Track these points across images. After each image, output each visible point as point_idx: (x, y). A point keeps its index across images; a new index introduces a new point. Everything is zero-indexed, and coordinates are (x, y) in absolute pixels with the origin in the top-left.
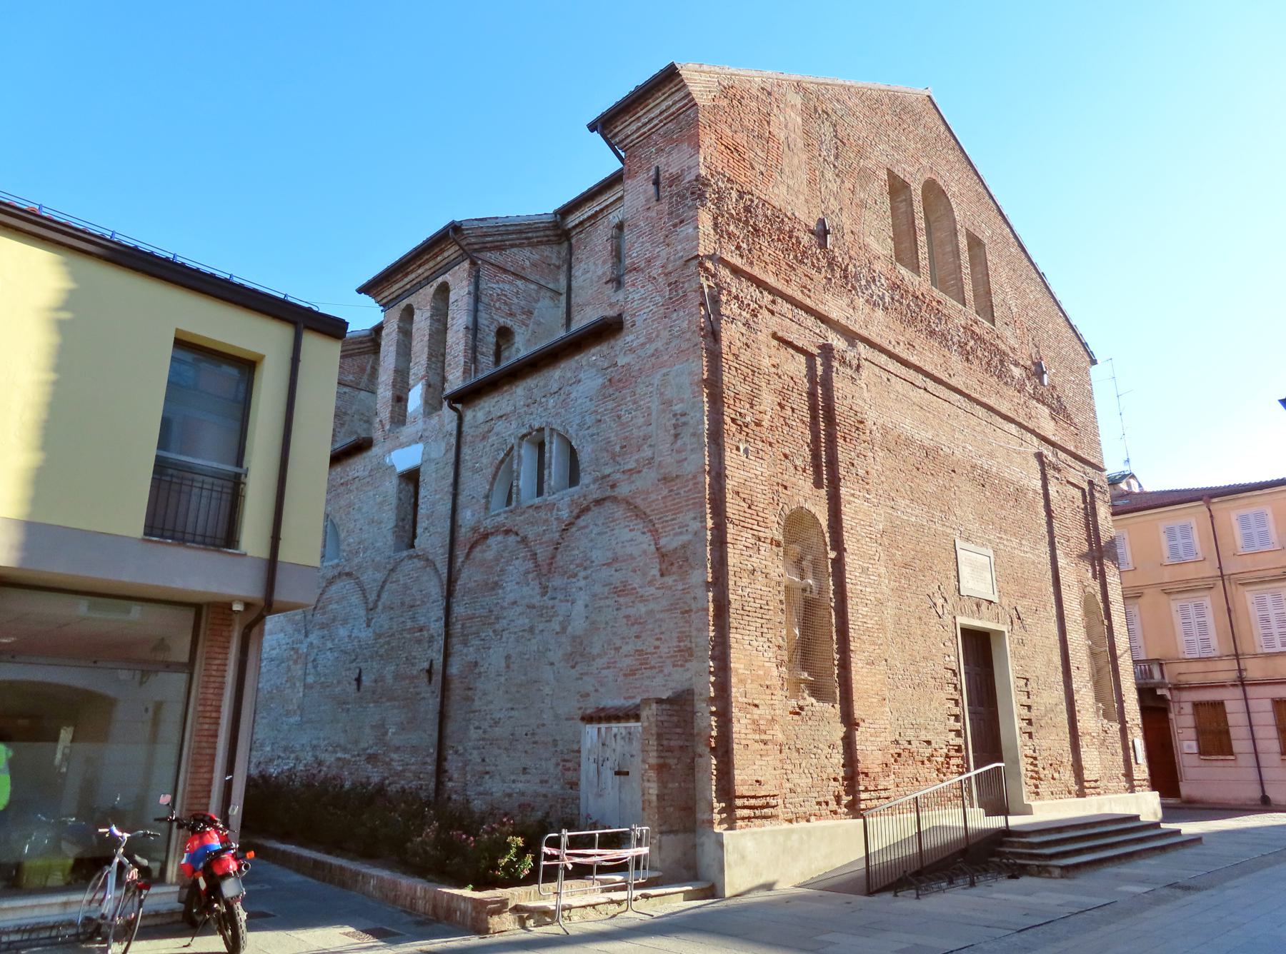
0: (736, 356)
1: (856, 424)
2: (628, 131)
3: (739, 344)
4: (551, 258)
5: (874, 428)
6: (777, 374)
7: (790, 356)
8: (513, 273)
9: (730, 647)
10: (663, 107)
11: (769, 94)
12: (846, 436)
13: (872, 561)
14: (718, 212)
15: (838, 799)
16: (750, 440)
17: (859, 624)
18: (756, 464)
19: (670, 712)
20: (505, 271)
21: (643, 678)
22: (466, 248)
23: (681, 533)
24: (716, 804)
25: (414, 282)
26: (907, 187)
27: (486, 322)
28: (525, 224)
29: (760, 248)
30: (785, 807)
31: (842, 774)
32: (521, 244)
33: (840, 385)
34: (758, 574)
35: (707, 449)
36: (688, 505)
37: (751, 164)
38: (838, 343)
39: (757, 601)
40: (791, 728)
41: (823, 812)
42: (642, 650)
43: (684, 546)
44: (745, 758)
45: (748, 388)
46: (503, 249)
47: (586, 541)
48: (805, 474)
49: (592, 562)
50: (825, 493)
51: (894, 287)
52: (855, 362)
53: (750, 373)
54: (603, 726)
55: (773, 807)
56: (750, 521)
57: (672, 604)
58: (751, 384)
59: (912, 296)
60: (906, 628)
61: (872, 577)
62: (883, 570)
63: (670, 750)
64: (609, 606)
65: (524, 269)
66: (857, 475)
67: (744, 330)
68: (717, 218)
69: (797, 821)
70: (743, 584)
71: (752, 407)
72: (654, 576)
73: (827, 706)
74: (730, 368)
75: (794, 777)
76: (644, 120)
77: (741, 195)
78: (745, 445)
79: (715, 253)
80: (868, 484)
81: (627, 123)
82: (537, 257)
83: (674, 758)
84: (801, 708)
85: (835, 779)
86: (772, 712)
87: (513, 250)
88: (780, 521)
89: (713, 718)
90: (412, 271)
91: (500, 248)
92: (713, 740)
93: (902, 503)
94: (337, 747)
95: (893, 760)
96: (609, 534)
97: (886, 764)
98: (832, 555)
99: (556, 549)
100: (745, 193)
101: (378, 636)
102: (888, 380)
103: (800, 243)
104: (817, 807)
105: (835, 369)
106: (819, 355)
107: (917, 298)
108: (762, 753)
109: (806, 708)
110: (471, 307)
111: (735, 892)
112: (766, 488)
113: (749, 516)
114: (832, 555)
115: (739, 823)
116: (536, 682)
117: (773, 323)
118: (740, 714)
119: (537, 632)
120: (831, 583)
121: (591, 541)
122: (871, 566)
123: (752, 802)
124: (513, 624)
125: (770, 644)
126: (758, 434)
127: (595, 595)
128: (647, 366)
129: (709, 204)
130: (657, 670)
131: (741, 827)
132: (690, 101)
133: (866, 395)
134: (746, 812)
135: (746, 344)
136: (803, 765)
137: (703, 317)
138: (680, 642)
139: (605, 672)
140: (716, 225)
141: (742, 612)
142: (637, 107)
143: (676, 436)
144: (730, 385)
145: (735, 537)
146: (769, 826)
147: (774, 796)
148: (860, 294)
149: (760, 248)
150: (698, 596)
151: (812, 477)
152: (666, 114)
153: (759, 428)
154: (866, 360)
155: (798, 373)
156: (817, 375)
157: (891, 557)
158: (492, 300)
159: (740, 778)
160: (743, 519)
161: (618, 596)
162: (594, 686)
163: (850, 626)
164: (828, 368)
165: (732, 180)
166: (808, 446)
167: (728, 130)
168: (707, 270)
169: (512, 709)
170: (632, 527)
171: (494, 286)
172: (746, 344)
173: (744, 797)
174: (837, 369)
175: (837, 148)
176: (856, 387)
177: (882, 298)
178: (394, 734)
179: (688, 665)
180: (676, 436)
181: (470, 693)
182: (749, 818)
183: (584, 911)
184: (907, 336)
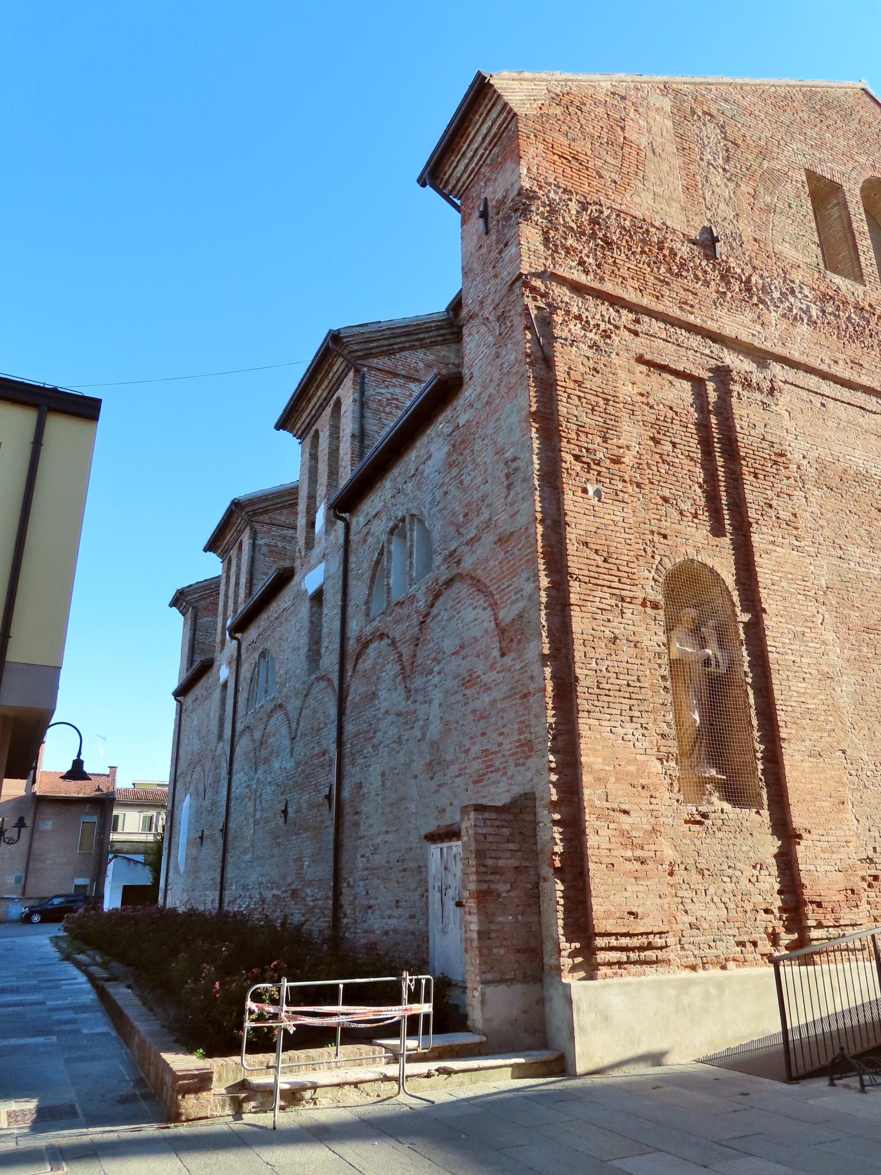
0: (579, 383)
1: (773, 457)
2: (457, 173)
3: (582, 369)
4: (449, 357)
5: (805, 462)
6: (648, 404)
7: (667, 384)
8: (404, 377)
9: (579, 736)
10: (484, 130)
11: (623, 98)
12: (757, 471)
13: (810, 624)
14: (549, 225)
15: (774, 939)
16: (602, 479)
17: (794, 704)
18: (614, 508)
19: (497, 823)
20: (395, 375)
21: (489, 784)
22: (349, 357)
23: (517, 600)
24: (564, 944)
25: (317, 406)
26: (838, 189)
27: (375, 428)
28: (414, 325)
29: (614, 262)
30: (683, 948)
31: (778, 903)
32: (411, 346)
33: (744, 412)
34: (623, 644)
35: (537, 493)
36: (521, 565)
37: (598, 173)
38: (730, 359)
39: (621, 677)
40: (688, 842)
41: (749, 957)
42: (487, 750)
43: (520, 616)
44: (610, 881)
45: (600, 419)
46: (392, 354)
47: (439, 630)
48: (696, 521)
49: (444, 653)
50: (729, 542)
51: (825, 298)
52: (766, 385)
53: (601, 402)
54: (445, 845)
55: (661, 948)
56: (606, 577)
57: (512, 689)
58: (603, 415)
59: (854, 307)
60: (875, 709)
61: (811, 644)
62: (830, 636)
63: (496, 871)
64: (458, 702)
65: (417, 371)
66: (778, 518)
67: (590, 353)
68: (547, 232)
69: (704, 968)
70: (598, 656)
71: (605, 442)
72: (495, 657)
73: (749, 813)
74: (569, 397)
75: (697, 909)
76: (470, 154)
77: (584, 206)
78: (596, 487)
79: (545, 271)
80: (796, 528)
81: (454, 164)
82: (432, 357)
83: (506, 882)
84: (705, 816)
85: (767, 911)
86: (653, 821)
87: (404, 353)
88: (656, 577)
89: (555, 829)
90: (313, 396)
91: (389, 352)
92: (557, 858)
93: (855, 552)
94: (275, 884)
95: (865, 885)
96: (457, 617)
97: (853, 891)
98: (745, 617)
99: (417, 645)
100: (590, 204)
101: (298, 764)
102: (823, 405)
103: (676, 255)
104: (738, 949)
105: (735, 394)
106: (710, 379)
107: (862, 309)
108: (637, 874)
109: (712, 816)
110: (357, 415)
111: (592, 1067)
112: (630, 536)
113: (606, 571)
114: (745, 617)
115: (604, 970)
116: (403, 799)
117: (639, 345)
118: (598, 823)
119: (404, 742)
120: (745, 653)
121: (443, 629)
122: (808, 630)
123: (625, 941)
124: (387, 736)
125: (644, 731)
126: (617, 473)
127: (447, 692)
128: (483, 417)
129: (536, 218)
130: (501, 773)
131: (606, 976)
132: (509, 113)
133: (787, 422)
134: (613, 956)
135: (595, 369)
136: (711, 891)
137: (529, 341)
138: (520, 734)
139: (457, 780)
140: (546, 241)
141: (597, 691)
142: (459, 142)
143: (509, 487)
144: (570, 416)
145: (583, 597)
146: (651, 974)
147: (661, 933)
148: (772, 308)
149: (614, 262)
150: (535, 674)
151: (708, 524)
152: (488, 139)
153: (617, 466)
154: (785, 382)
155: (680, 402)
156: (708, 403)
157: (844, 620)
158: (381, 406)
159: (602, 909)
160: (596, 575)
161: (466, 688)
162: (449, 799)
163: (778, 707)
164: (725, 394)
165: (570, 191)
166: (700, 487)
167: (562, 139)
168: (533, 289)
169: (387, 832)
170: (475, 605)
171: (383, 391)
172: (595, 369)
173: (610, 935)
174: (739, 393)
175: (727, 151)
176: (770, 414)
177: (807, 311)
178: (308, 866)
179: (529, 762)
180: (509, 487)
181: (356, 817)
182: (620, 964)
183: (338, 1093)
184: (849, 354)
